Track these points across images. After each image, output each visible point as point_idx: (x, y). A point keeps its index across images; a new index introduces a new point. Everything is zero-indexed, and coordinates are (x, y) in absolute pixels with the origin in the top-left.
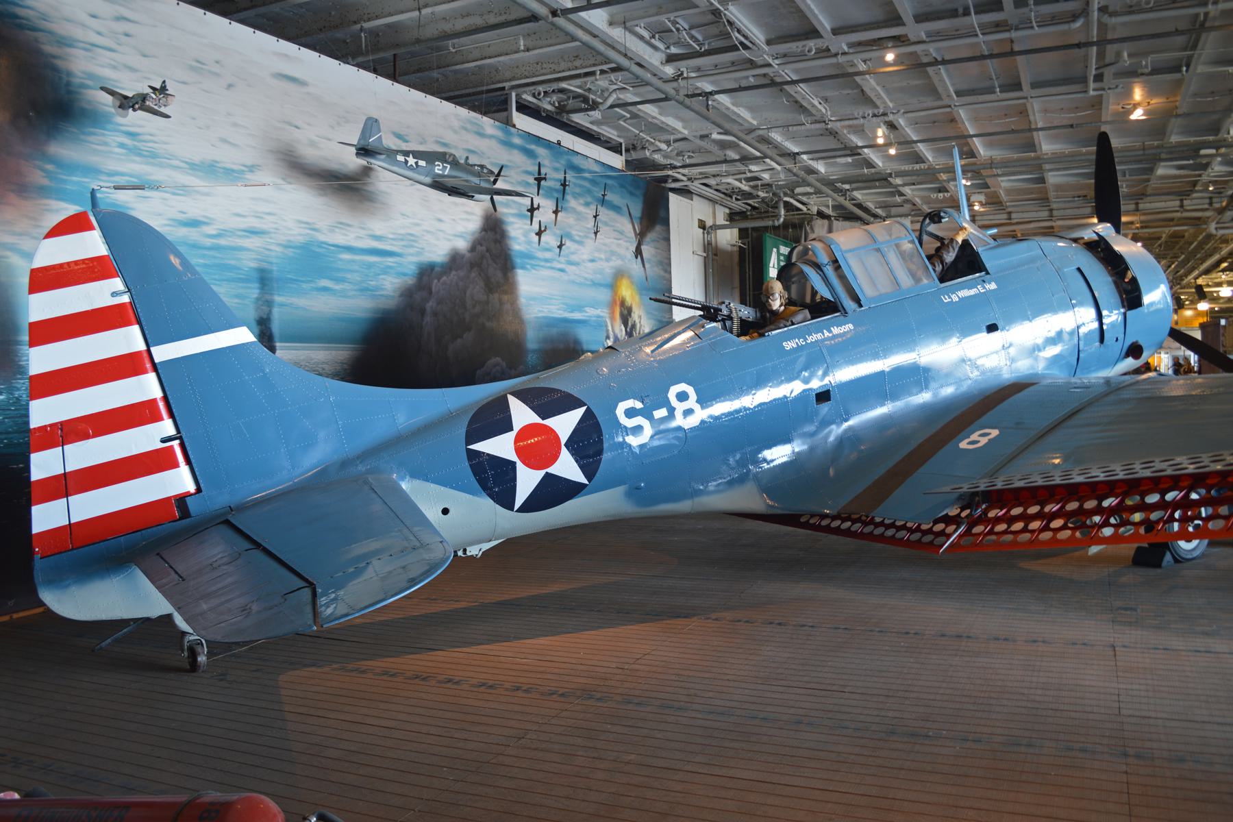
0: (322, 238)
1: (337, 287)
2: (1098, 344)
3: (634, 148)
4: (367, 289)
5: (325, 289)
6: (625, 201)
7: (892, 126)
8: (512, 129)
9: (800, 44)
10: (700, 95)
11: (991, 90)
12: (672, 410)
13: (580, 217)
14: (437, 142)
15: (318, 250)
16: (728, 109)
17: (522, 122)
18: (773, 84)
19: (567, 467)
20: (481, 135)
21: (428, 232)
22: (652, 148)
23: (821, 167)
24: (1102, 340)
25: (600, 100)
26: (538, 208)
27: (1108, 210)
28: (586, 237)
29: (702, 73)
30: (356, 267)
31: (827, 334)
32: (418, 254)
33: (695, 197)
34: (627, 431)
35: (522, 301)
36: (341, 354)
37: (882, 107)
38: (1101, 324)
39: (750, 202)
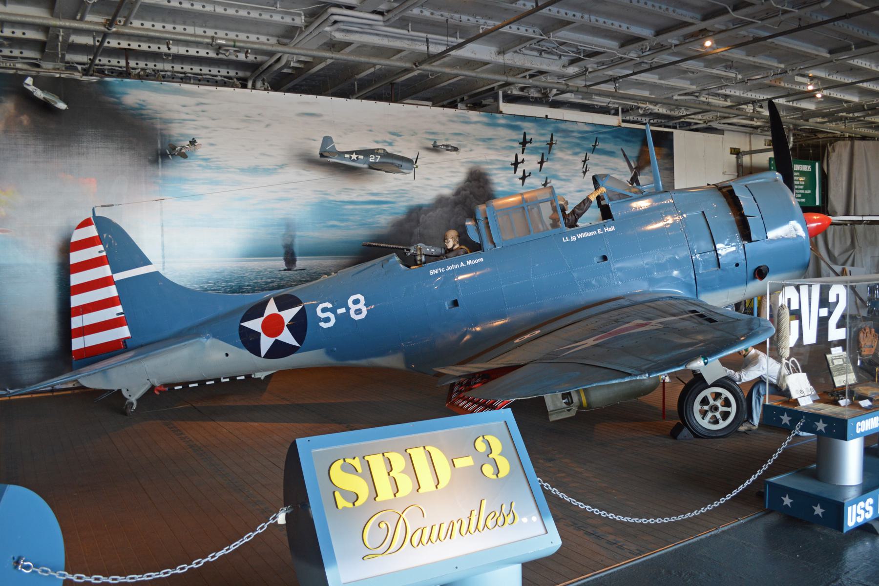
0: (331, 198)
1: (342, 224)
6: (620, 147)
12: (348, 309)
13: (566, 163)
14: (426, 133)
17: (507, 108)
19: (286, 337)
20: (467, 122)
26: (523, 161)
31: (462, 264)
33: (726, 132)
34: (320, 320)
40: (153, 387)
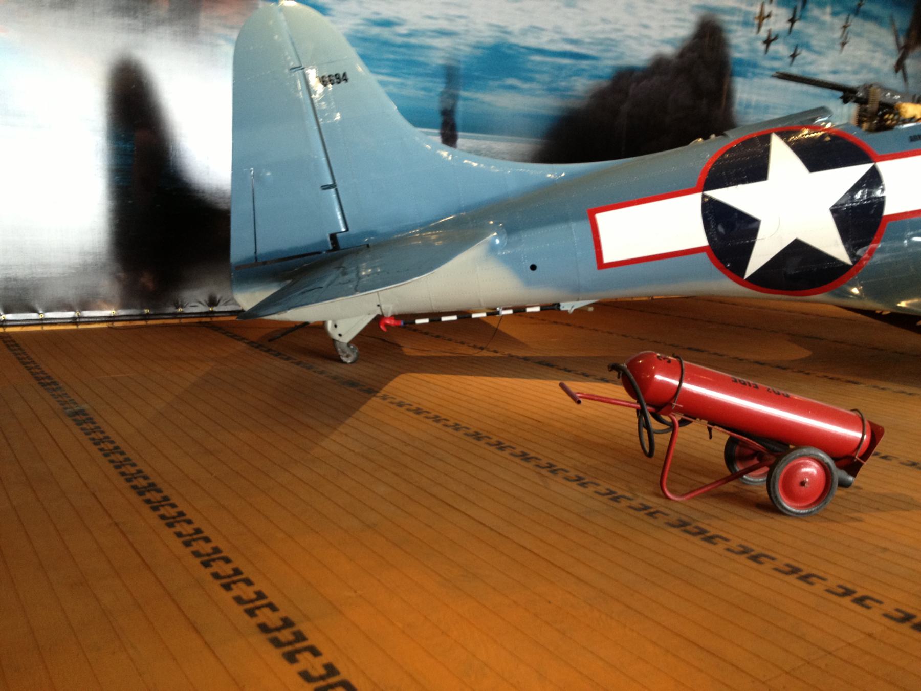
0: (513, 40)
4: (556, 89)
5: (512, 87)
13: (821, 25)
21: (630, 37)
26: (769, 16)
28: (828, 48)
30: (545, 69)
32: (616, 58)
40: (379, 319)
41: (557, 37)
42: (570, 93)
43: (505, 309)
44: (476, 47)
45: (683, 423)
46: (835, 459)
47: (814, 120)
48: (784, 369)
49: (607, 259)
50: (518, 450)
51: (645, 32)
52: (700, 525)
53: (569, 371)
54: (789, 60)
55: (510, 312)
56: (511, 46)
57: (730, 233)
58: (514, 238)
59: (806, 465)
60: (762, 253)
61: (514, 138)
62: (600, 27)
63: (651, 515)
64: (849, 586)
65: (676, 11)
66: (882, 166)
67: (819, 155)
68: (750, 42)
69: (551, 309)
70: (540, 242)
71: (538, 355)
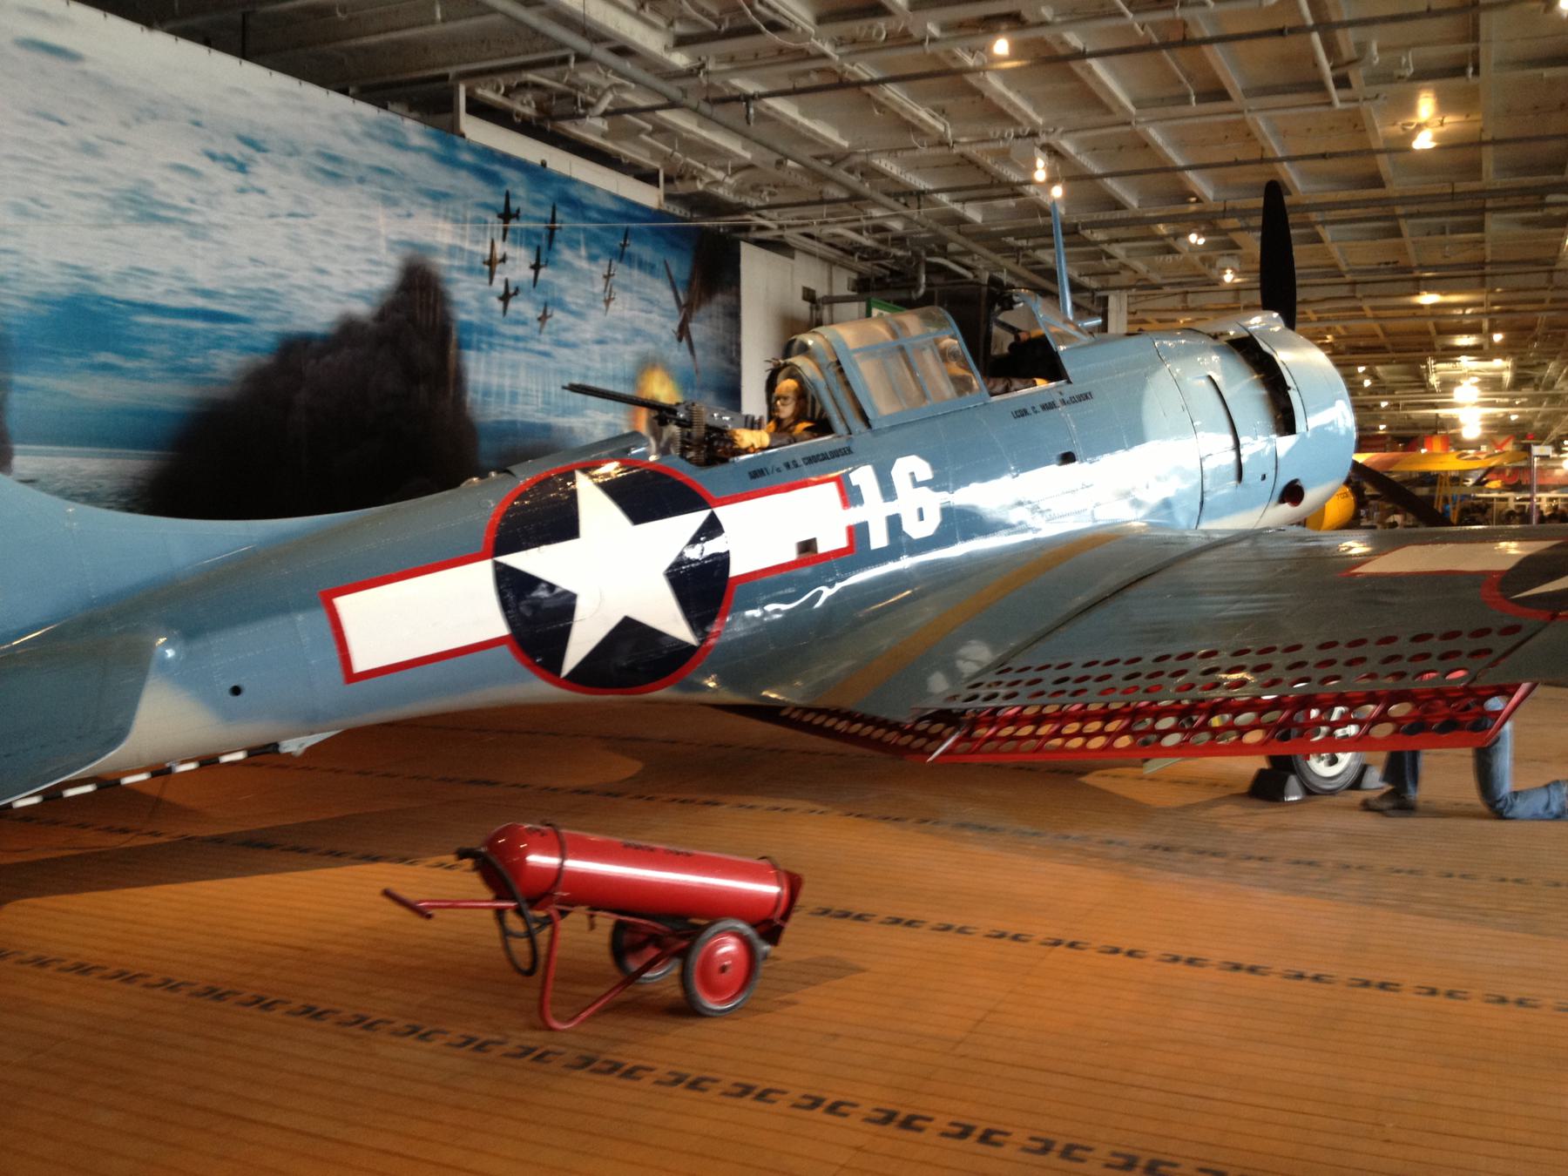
0: (102, 290)
2: (1233, 483)
3: (681, 177)
4: (184, 370)
5: (106, 367)
7: (1053, 152)
8: (459, 140)
9: (865, 23)
10: (737, 99)
11: (1184, 99)
15: (94, 308)
16: (794, 122)
17: (477, 131)
18: (842, 84)
20: (401, 145)
21: (301, 288)
22: (707, 180)
23: (974, 213)
24: (1240, 477)
25: (593, 100)
26: (504, 260)
27: (1278, 291)
28: (589, 306)
29: (740, 64)
30: (164, 336)
32: (277, 321)
33: (798, 255)
35: (471, 397)
36: (132, 465)
37: (1025, 123)
38: (1239, 456)
39: (883, 262)
41: (178, 285)
42: (210, 375)
43: (183, 762)
44: (41, 300)
45: (563, 914)
46: (754, 926)
47: (628, 451)
48: (617, 795)
49: (360, 665)
50: (297, 1004)
51: (325, 280)
52: (611, 1058)
53: (306, 851)
54: (537, 325)
55: (192, 766)
56: (101, 300)
57: (537, 617)
58: (198, 645)
59: (723, 943)
60: (583, 640)
61: (116, 451)
62: (251, 270)
63: (540, 1058)
64: (815, 1093)
65: (365, 250)
66: (722, 513)
67: (644, 498)
68: (481, 298)
69: (265, 753)
70: (245, 649)
71: (232, 829)
